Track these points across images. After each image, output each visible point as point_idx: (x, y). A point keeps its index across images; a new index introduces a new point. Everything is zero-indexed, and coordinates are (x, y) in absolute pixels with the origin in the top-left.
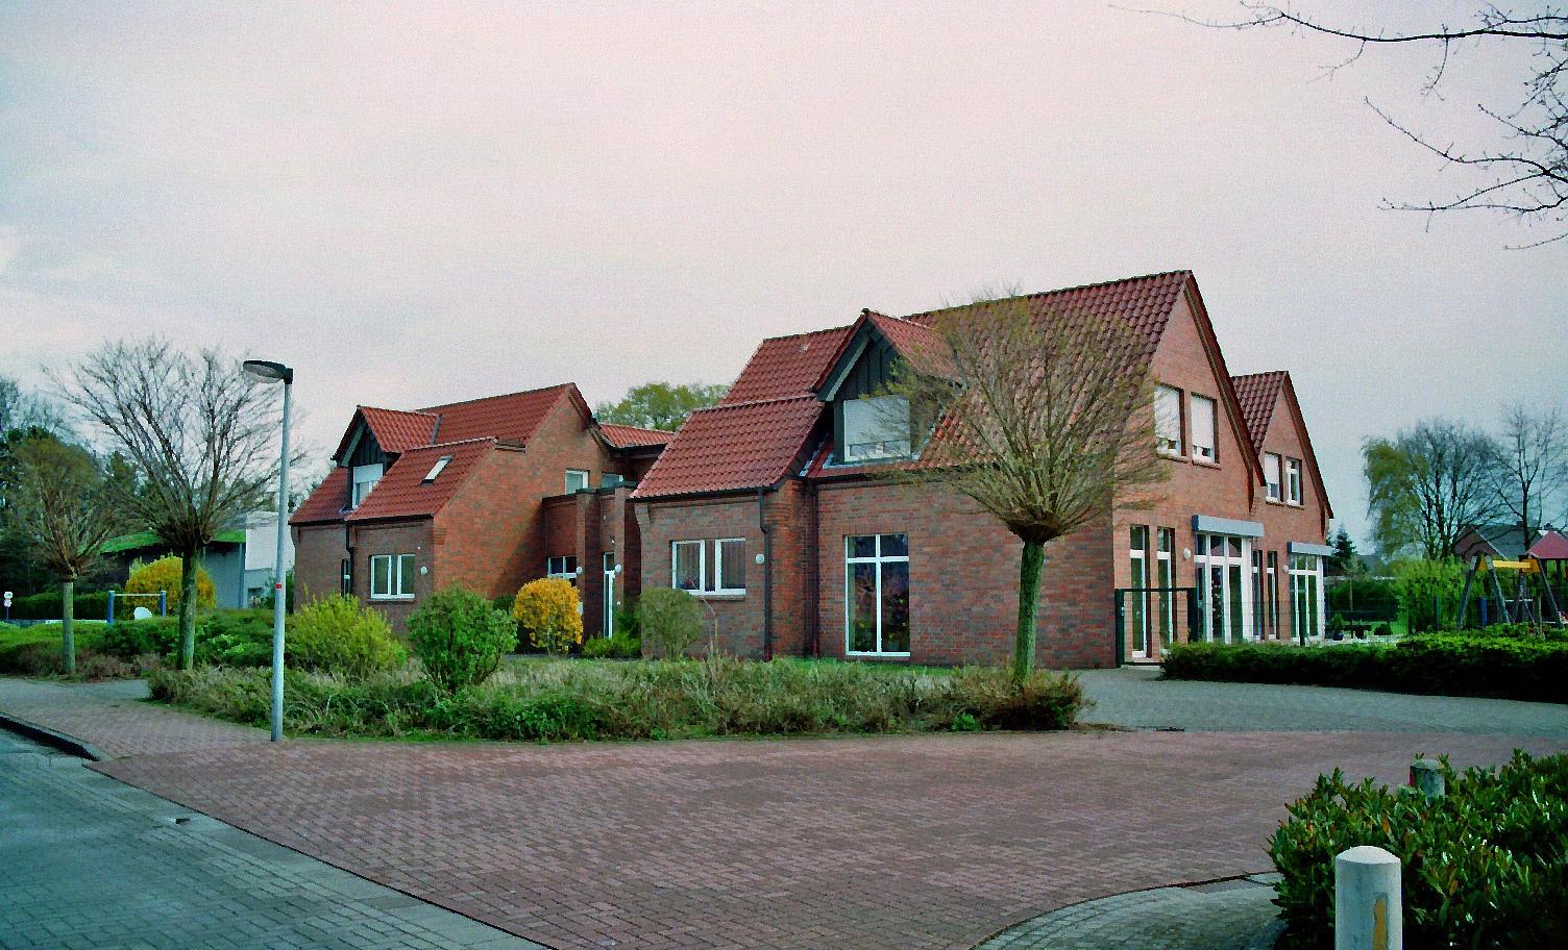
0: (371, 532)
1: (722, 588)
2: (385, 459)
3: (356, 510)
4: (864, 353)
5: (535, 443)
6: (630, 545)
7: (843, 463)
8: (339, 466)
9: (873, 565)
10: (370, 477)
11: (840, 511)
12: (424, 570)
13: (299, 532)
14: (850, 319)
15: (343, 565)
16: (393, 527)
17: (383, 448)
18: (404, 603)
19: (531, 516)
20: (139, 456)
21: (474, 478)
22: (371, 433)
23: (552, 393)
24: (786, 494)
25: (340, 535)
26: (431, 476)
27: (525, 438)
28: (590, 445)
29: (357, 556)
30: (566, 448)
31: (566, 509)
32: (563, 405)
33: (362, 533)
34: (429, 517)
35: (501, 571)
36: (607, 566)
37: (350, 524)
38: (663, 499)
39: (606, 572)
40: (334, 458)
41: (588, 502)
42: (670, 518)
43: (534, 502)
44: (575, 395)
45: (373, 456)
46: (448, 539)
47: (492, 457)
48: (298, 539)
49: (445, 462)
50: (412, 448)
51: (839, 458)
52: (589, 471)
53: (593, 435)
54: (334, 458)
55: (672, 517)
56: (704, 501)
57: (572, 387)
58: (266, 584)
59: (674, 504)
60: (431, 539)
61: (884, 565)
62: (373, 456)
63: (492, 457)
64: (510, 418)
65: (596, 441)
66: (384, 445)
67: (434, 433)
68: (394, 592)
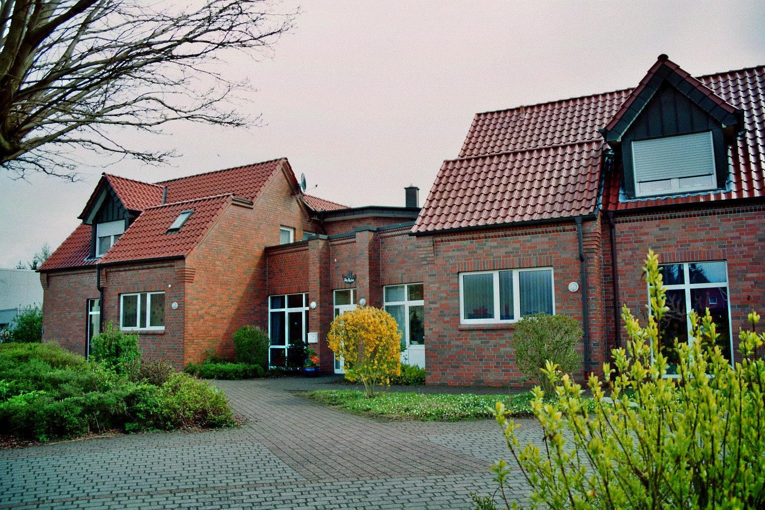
0: (121, 273)
1: (691, 290)
2: (127, 215)
3: (100, 257)
4: (668, 99)
5: (258, 202)
6: (373, 281)
7: (635, 198)
8: (84, 223)
9: (693, 291)
10: (111, 230)
11: (642, 241)
12: (175, 305)
13: (48, 278)
14: (632, 76)
15: (87, 302)
16: (143, 269)
17: (126, 207)
18: (154, 334)
19: (257, 261)
20: (112, 108)
21: (216, 227)
22: (115, 194)
23: (267, 167)
24: (595, 227)
25: (90, 280)
26: (177, 224)
27: (253, 198)
28: (295, 208)
29: (106, 294)
30: (281, 209)
31: (290, 255)
32: (277, 175)
33: (111, 275)
34: (182, 258)
35: (236, 307)
36: (387, 297)
37: (101, 267)
38: (443, 232)
39: (335, 307)
40: (80, 218)
41: (321, 247)
42: (458, 250)
43: (258, 251)
44: (287, 168)
45: (116, 214)
46: (196, 278)
47: (228, 210)
48: (47, 284)
49: (186, 216)
50: (148, 208)
51: (630, 191)
52: (294, 229)
53: (297, 201)
54: (80, 218)
55: (459, 249)
56: (501, 233)
57: (285, 161)
58: (14, 320)
59: (463, 236)
60: (183, 278)
61: (683, 291)
62: (116, 214)
63: (228, 210)
64: (240, 184)
65: (299, 204)
66: (128, 202)
67: (163, 196)
68: (143, 325)
